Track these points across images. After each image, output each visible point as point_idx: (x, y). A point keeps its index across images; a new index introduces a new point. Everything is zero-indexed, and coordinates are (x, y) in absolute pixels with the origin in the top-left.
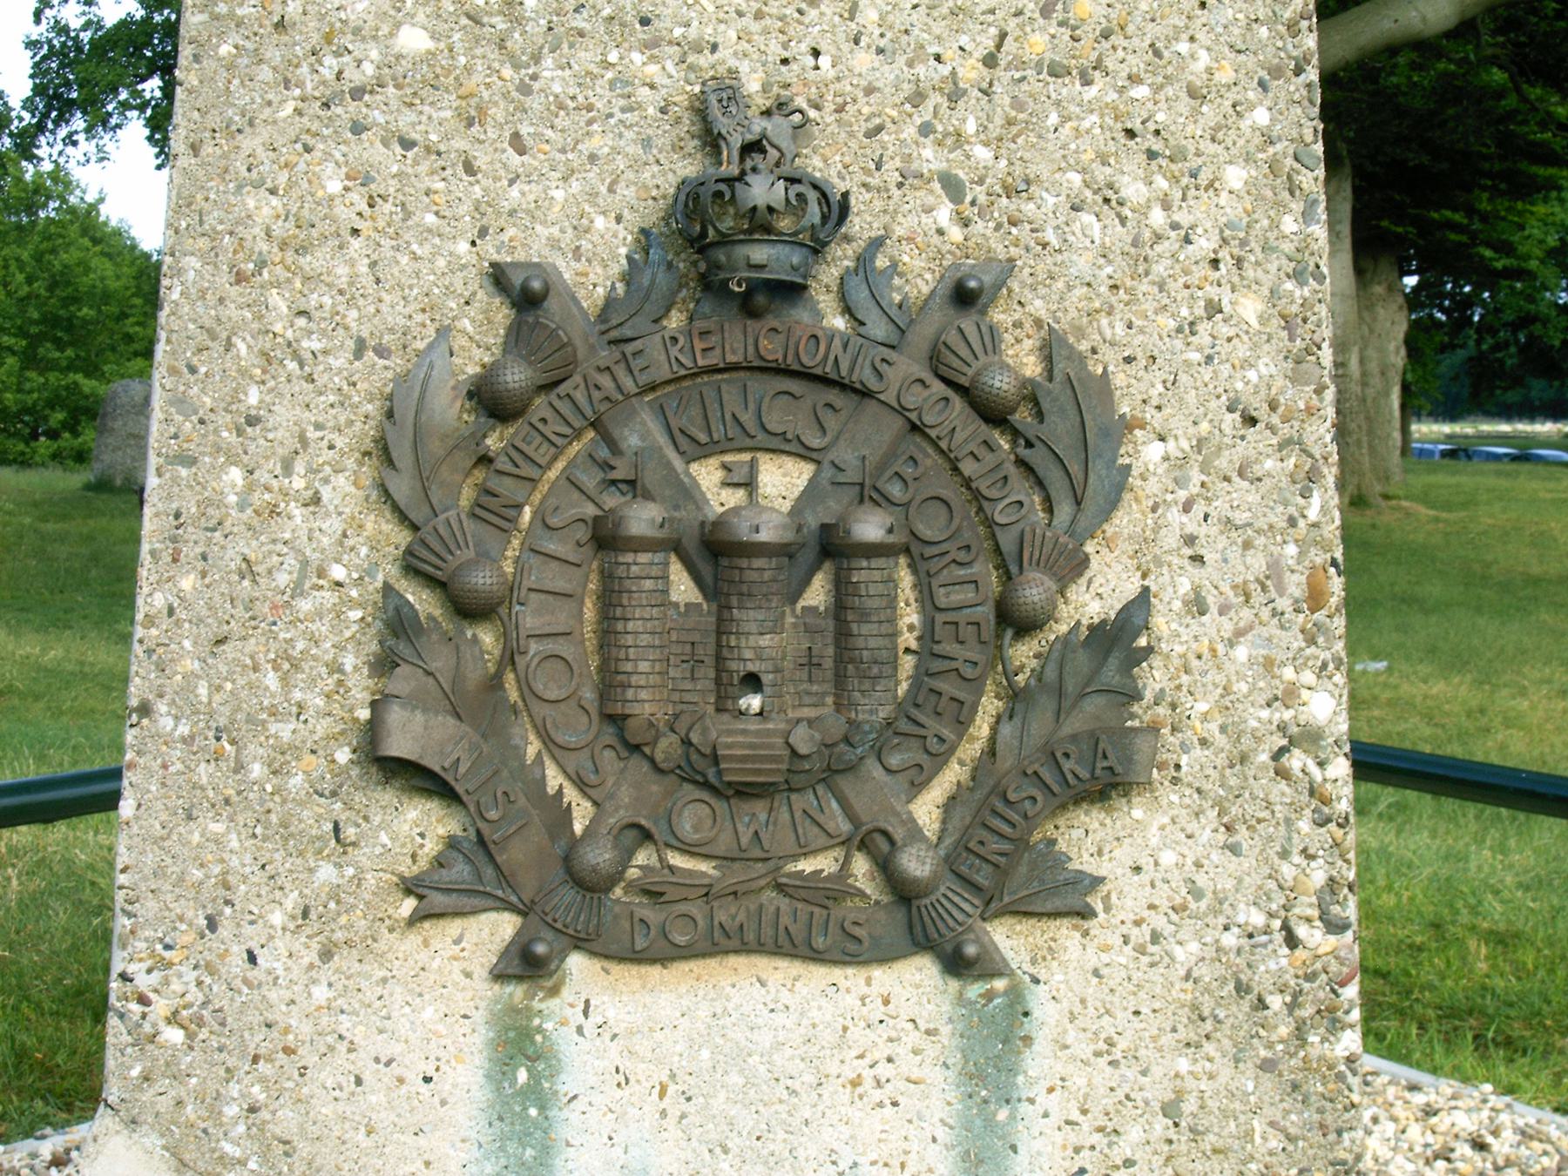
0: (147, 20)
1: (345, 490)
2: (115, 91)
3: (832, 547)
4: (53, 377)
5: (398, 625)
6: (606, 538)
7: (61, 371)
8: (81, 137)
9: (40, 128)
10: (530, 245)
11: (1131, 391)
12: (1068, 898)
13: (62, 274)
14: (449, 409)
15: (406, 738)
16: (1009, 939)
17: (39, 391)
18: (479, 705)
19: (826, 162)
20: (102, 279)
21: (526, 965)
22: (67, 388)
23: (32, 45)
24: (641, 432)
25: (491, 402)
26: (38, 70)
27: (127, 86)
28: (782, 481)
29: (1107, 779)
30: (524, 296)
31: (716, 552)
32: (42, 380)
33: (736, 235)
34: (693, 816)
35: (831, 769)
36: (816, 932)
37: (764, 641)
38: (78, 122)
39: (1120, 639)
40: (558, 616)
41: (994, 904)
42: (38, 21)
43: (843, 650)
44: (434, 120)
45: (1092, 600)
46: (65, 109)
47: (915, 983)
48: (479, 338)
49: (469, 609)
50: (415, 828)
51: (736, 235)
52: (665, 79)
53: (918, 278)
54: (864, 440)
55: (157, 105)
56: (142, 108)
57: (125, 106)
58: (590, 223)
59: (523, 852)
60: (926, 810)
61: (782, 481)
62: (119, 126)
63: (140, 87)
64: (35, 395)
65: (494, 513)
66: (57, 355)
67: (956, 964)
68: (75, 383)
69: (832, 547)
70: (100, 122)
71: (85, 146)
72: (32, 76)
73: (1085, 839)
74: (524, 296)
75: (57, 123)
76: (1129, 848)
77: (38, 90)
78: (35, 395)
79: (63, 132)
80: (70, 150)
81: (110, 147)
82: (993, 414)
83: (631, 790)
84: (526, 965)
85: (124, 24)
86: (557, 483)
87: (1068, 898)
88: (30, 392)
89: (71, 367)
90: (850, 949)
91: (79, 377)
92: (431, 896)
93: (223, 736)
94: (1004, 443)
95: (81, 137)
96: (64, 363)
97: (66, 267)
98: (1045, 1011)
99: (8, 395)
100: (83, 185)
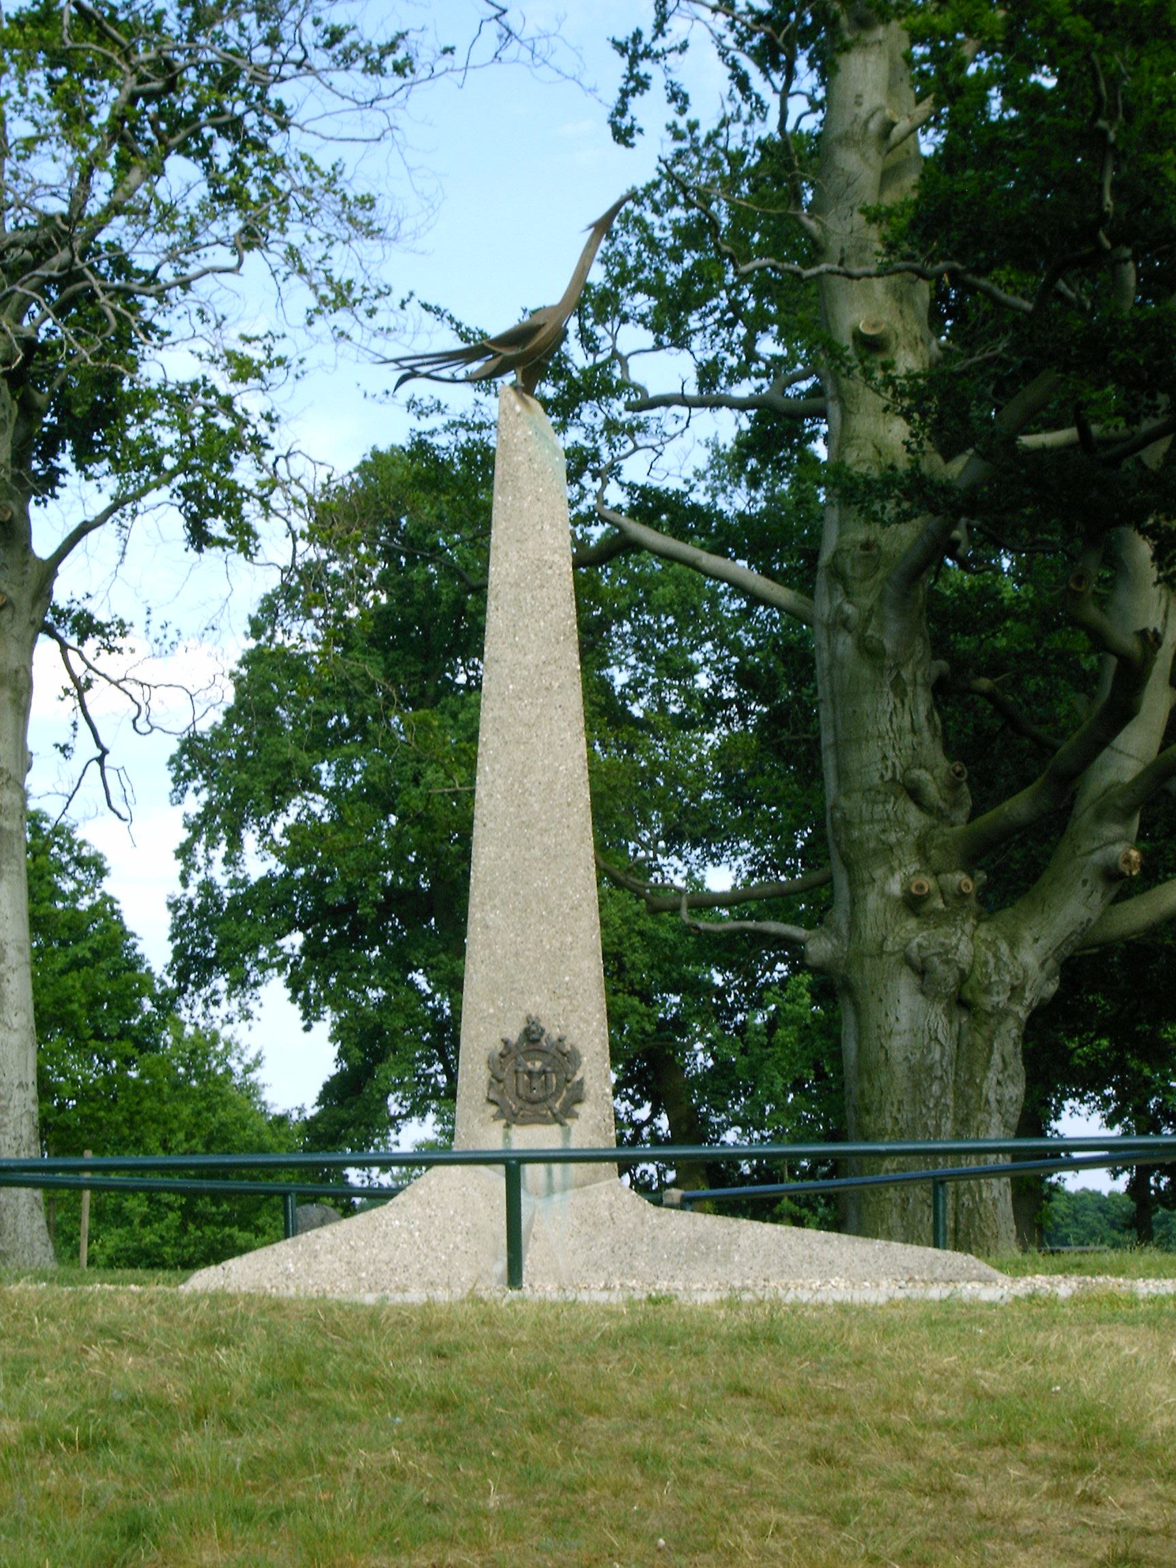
0: (287, 876)
1: (484, 1067)
2: (255, 948)
3: (545, 1072)
4: (208, 1231)
5: (491, 1083)
6: (516, 1072)
7: (217, 1224)
8: (223, 996)
9: (181, 991)
10: (507, 1036)
11: (582, 1051)
12: (576, 1116)
13: (219, 1130)
14: (497, 1056)
15: (492, 1097)
16: (568, 1121)
17: (195, 1245)
18: (501, 1093)
19: (542, 1024)
20: (259, 1134)
21: (508, 1126)
22: (222, 1242)
23: (174, 906)
24: (521, 1058)
25: (502, 1055)
26: (177, 932)
27: (266, 944)
28: (538, 1064)
29: (579, 1101)
30: (506, 1042)
31: (530, 1073)
32: (199, 1233)
33: (532, 1035)
34: (528, 1106)
35: (545, 1100)
36: (544, 1121)
37: (536, 1084)
38: (221, 983)
39: (581, 1083)
40: (510, 1081)
41: (566, 1116)
42: (185, 884)
43: (546, 1085)
44: (494, 1021)
45: (577, 1078)
46: (207, 967)
47: (556, 1128)
48: (500, 1048)
49: (499, 1081)
50: (493, 1109)
51: (532, 1035)
52: (522, 1015)
53: (555, 1038)
54: (548, 1058)
55: (296, 963)
56: (281, 966)
57: (264, 966)
58: (514, 1033)
59: (507, 1111)
60: (557, 1105)
61: (538, 1064)
62: (256, 984)
63: (280, 943)
64: (192, 1249)
65: (503, 1069)
66: (214, 1209)
67: (562, 1124)
68: (231, 1236)
69: (545, 1072)
70: (240, 983)
71: (228, 1006)
72: (172, 939)
73: (577, 1108)
74: (506, 1042)
75: (198, 986)
76: (583, 1109)
77: (179, 952)
78: (192, 1249)
79: (205, 991)
80: (213, 1010)
81: (253, 1006)
82: (564, 1055)
83: (520, 1103)
84: (508, 1126)
85: (265, 882)
86: (510, 1065)
87: (576, 1116)
88: (185, 1247)
89: (227, 1221)
90: (548, 1123)
91: (235, 1231)
92: (496, 1118)
93: (469, 1098)
94: (564, 1058)
95: (223, 996)
96: (220, 1218)
97: (223, 1124)
98: (573, 1130)
99: (168, 1249)
100: (243, 1045)
